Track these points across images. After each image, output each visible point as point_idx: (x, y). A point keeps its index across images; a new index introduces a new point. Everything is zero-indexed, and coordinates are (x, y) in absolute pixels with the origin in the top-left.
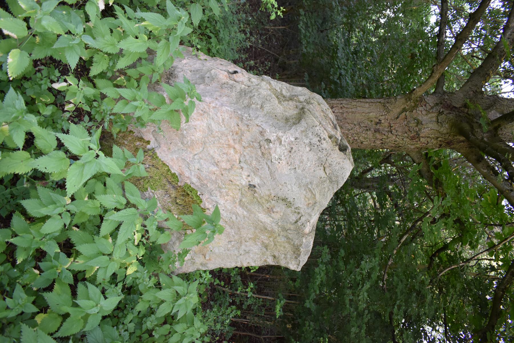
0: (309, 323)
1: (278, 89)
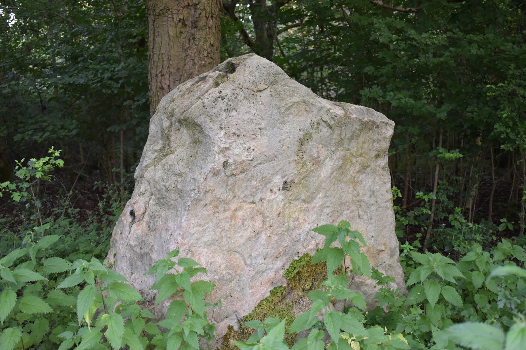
0: (468, 112)
1: (153, 156)
